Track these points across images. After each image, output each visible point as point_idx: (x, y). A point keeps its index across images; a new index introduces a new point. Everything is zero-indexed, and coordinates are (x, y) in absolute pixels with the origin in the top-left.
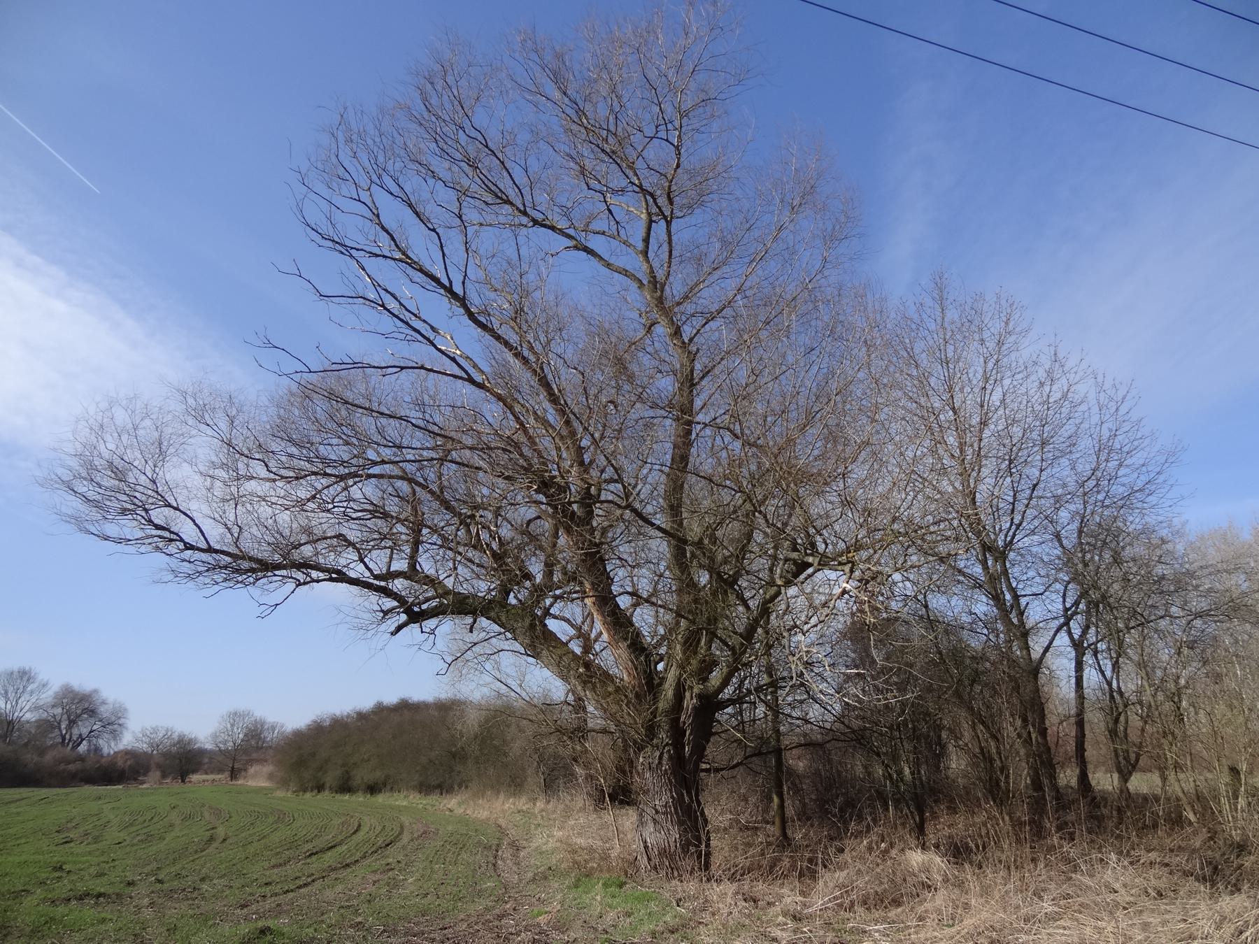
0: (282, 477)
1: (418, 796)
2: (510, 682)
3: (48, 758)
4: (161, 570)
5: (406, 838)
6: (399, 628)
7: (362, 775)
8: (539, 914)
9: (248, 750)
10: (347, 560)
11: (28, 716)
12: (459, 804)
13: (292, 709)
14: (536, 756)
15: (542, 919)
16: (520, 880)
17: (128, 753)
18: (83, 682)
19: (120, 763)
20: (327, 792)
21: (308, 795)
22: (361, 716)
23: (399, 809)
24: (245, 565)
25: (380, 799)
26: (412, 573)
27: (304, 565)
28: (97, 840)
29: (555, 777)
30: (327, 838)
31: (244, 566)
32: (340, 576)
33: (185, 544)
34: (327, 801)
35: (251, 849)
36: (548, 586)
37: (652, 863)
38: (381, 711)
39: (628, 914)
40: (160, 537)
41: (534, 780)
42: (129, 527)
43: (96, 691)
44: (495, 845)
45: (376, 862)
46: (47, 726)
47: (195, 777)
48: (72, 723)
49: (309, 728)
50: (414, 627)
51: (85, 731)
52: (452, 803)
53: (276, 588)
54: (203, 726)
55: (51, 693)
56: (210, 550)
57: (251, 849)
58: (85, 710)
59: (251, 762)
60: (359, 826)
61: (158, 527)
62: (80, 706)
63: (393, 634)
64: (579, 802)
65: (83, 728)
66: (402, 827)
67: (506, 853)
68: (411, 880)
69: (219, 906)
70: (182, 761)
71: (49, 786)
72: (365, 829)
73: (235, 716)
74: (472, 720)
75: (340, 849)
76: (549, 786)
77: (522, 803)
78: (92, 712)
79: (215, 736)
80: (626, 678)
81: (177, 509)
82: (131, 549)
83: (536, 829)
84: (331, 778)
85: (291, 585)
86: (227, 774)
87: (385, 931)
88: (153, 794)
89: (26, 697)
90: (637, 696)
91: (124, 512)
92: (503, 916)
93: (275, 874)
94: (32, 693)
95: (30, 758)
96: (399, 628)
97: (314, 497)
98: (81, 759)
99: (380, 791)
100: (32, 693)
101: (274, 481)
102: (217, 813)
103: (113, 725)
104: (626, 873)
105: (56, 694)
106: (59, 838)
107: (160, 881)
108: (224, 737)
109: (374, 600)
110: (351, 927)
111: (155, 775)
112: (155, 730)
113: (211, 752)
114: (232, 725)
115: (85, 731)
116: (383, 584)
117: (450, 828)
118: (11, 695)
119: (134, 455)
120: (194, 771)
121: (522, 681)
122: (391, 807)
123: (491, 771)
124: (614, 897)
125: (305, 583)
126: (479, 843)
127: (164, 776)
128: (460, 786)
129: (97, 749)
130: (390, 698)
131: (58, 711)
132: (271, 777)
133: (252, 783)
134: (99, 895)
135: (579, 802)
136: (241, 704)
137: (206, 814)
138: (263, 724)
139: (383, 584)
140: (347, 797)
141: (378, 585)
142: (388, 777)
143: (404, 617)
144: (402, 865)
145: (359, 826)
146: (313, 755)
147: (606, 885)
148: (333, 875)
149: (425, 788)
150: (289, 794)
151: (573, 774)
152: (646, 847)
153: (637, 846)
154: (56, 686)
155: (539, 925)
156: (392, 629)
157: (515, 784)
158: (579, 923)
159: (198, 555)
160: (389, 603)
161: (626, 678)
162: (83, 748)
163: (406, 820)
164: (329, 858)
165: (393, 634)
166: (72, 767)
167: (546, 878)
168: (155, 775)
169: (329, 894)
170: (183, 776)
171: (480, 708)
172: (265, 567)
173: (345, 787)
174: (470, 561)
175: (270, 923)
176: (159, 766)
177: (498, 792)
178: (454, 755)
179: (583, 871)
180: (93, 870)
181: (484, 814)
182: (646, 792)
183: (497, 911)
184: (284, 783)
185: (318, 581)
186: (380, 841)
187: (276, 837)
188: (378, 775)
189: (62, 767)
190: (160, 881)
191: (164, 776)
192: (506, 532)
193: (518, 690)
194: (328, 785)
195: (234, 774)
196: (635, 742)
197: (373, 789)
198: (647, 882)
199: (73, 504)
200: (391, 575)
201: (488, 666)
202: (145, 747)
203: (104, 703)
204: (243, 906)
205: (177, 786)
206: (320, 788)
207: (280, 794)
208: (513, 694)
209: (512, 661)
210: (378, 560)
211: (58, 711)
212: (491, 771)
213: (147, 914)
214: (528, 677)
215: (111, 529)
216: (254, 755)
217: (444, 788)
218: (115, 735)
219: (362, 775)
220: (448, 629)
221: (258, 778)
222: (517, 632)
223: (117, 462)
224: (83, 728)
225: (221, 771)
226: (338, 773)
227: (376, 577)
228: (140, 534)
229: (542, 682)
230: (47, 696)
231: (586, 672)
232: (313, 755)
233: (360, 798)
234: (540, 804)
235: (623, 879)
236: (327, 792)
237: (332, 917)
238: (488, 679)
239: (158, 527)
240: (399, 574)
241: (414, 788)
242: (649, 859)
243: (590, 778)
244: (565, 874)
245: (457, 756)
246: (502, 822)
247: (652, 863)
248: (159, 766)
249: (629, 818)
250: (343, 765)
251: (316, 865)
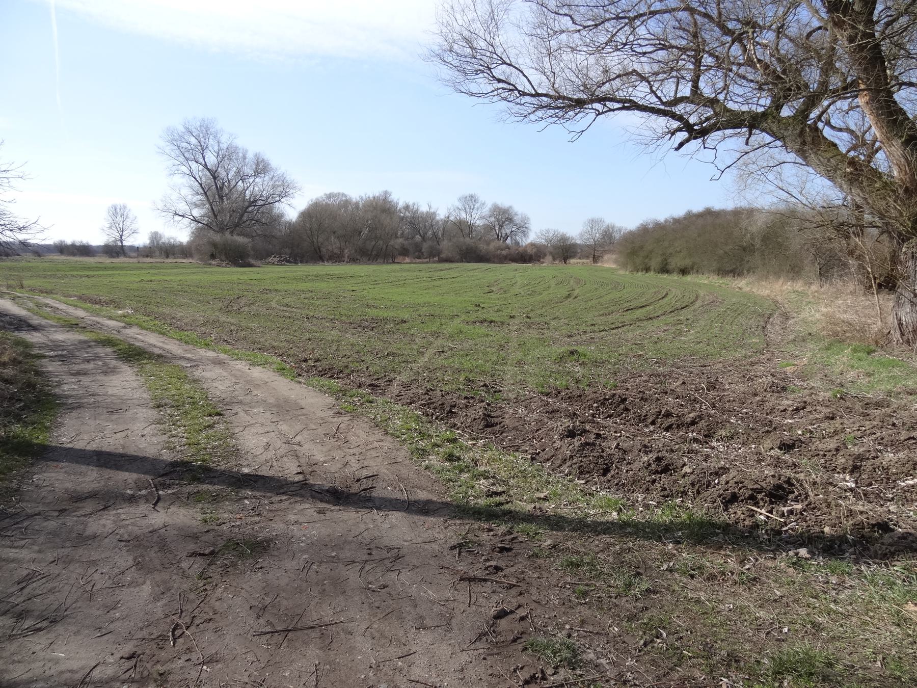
0: (585, 27)
1: (716, 277)
2: (791, 189)
3: (492, 246)
4: (502, 112)
5: (697, 304)
6: (681, 145)
7: (676, 262)
8: (787, 365)
9: (601, 246)
10: (640, 93)
11: (478, 222)
12: (747, 284)
13: (628, 216)
14: (813, 251)
15: (789, 370)
16: (782, 340)
17: (532, 245)
18: (504, 202)
19: (529, 251)
20: (652, 272)
21: (640, 274)
22: (676, 221)
23: (700, 286)
24: (559, 103)
25: (689, 278)
26: (696, 96)
27: (602, 100)
28: (505, 292)
29: (829, 267)
30: (642, 301)
31: (565, 105)
32: (631, 105)
33: (519, 91)
34: (651, 277)
35: (590, 304)
36: (824, 89)
37: (905, 338)
38: (691, 219)
39: (869, 375)
40: (503, 89)
41: (812, 269)
42: (482, 84)
43: (511, 207)
44: (767, 314)
45: (670, 319)
46: (489, 228)
47: (572, 261)
48: (501, 226)
49: (638, 229)
50: (695, 144)
51: (508, 231)
52: (742, 284)
53: (585, 118)
54: (574, 229)
55: (487, 209)
56: (537, 95)
57: (590, 304)
58: (507, 219)
59: (606, 252)
60: (667, 294)
61: (499, 81)
62: (503, 217)
63: (677, 149)
64: (851, 287)
65: (507, 230)
66: (697, 297)
67: (776, 320)
68: (692, 332)
69: (556, 335)
70: (564, 251)
71: (494, 262)
72: (670, 296)
73: (593, 222)
74: (759, 224)
75: (648, 308)
76: (824, 273)
77: (799, 286)
78: (510, 220)
79: (581, 235)
80: (896, 173)
81: (510, 65)
82: (486, 100)
83: (807, 305)
84: (655, 262)
85: (592, 115)
86: (591, 259)
87: (657, 362)
88: (546, 270)
89: (475, 211)
90: (907, 190)
91: (477, 72)
92: (756, 363)
93: (598, 320)
94: (478, 209)
95: (482, 247)
96: (681, 145)
97: (610, 40)
98: (508, 247)
99: (689, 273)
100: (478, 209)
101: (579, 31)
102: (578, 281)
103: (523, 228)
104: (882, 341)
105: (490, 209)
106: (487, 289)
107: (529, 317)
108: (586, 236)
109: (662, 123)
110: (634, 357)
111: (549, 258)
112: (548, 231)
113: (579, 245)
114: (592, 228)
115: (508, 231)
116: (668, 108)
117: (734, 300)
118: (468, 210)
119: (478, 27)
120: (571, 257)
121: (802, 189)
122: (695, 284)
123: (774, 262)
124: (860, 360)
125: (603, 113)
126: (755, 312)
127: (554, 259)
128: (748, 272)
129: (517, 243)
130: (698, 208)
131: (493, 219)
132: (616, 261)
133: (606, 265)
134: (491, 322)
135: (851, 287)
136: (596, 215)
137: (572, 282)
138: (613, 227)
139: (668, 108)
140: (666, 276)
141: (665, 110)
142: (694, 264)
143: (683, 135)
144: (690, 322)
145: (667, 294)
146: (642, 247)
147: (855, 350)
148: (638, 324)
149: (722, 272)
150: (627, 273)
151: (845, 265)
152: (900, 324)
153: (891, 320)
154: (489, 205)
155: (785, 373)
156: (676, 145)
157: (795, 271)
158: (820, 376)
159: (527, 99)
160: (675, 124)
161: (896, 173)
162: (509, 241)
163: (702, 293)
164: (639, 313)
165: (677, 149)
166: (504, 252)
167: (804, 341)
168: (549, 258)
169: (630, 335)
170: (565, 259)
171: (770, 212)
172: (580, 104)
173: (664, 269)
174: (744, 78)
175: (580, 349)
176: (551, 253)
177: (780, 277)
178: (744, 249)
179: (836, 337)
180: (495, 308)
181: (765, 292)
182: (906, 278)
183: (752, 360)
184: (624, 266)
185: (614, 110)
186: (678, 305)
187: (607, 298)
188: (687, 262)
189: (499, 252)
190: (529, 317)
191: (554, 259)
192: (786, 46)
193: (799, 197)
194: (652, 268)
195: (595, 259)
196: (900, 234)
197: (684, 272)
198: (896, 352)
199: (447, 73)
200: (677, 101)
201: (771, 176)
202: (544, 242)
203: (516, 214)
204: (570, 336)
205: (559, 265)
206: (647, 270)
207: (622, 272)
208: (793, 200)
209: (794, 172)
210: (668, 90)
211: (493, 219)
212: (774, 262)
213: (514, 334)
214: (808, 185)
215: (474, 88)
216: (606, 248)
217: (735, 272)
218: (525, 234)
219: (676, 262)
220: (728, 144)
221: (609, 263)
222: (787, 140)
223: (466, 33)
224: (507, 230)
225: (588, 257)
226: (659, 259)
227: (663, 103)
228: (490, 88)
229: (818, 189)
230: (486, 211)
231: (856, 171)
232: (642, 247)
233: (675, 277)
234: (814, 288)
235: (873, 347)
236: (652, 272)
237: (623, 350)
238: (772, 188)
239: (499, 81)
240: (683, 99)
241: (714, 271)
242: (902, 334)
243: (861, 267)
244: (820, 339)
245: (748, 249)
246: (779, 298)
247: (905, 338)
248: (551, 253)
249: (886, 301)
250: (663, 254)
251: (629, 316)
